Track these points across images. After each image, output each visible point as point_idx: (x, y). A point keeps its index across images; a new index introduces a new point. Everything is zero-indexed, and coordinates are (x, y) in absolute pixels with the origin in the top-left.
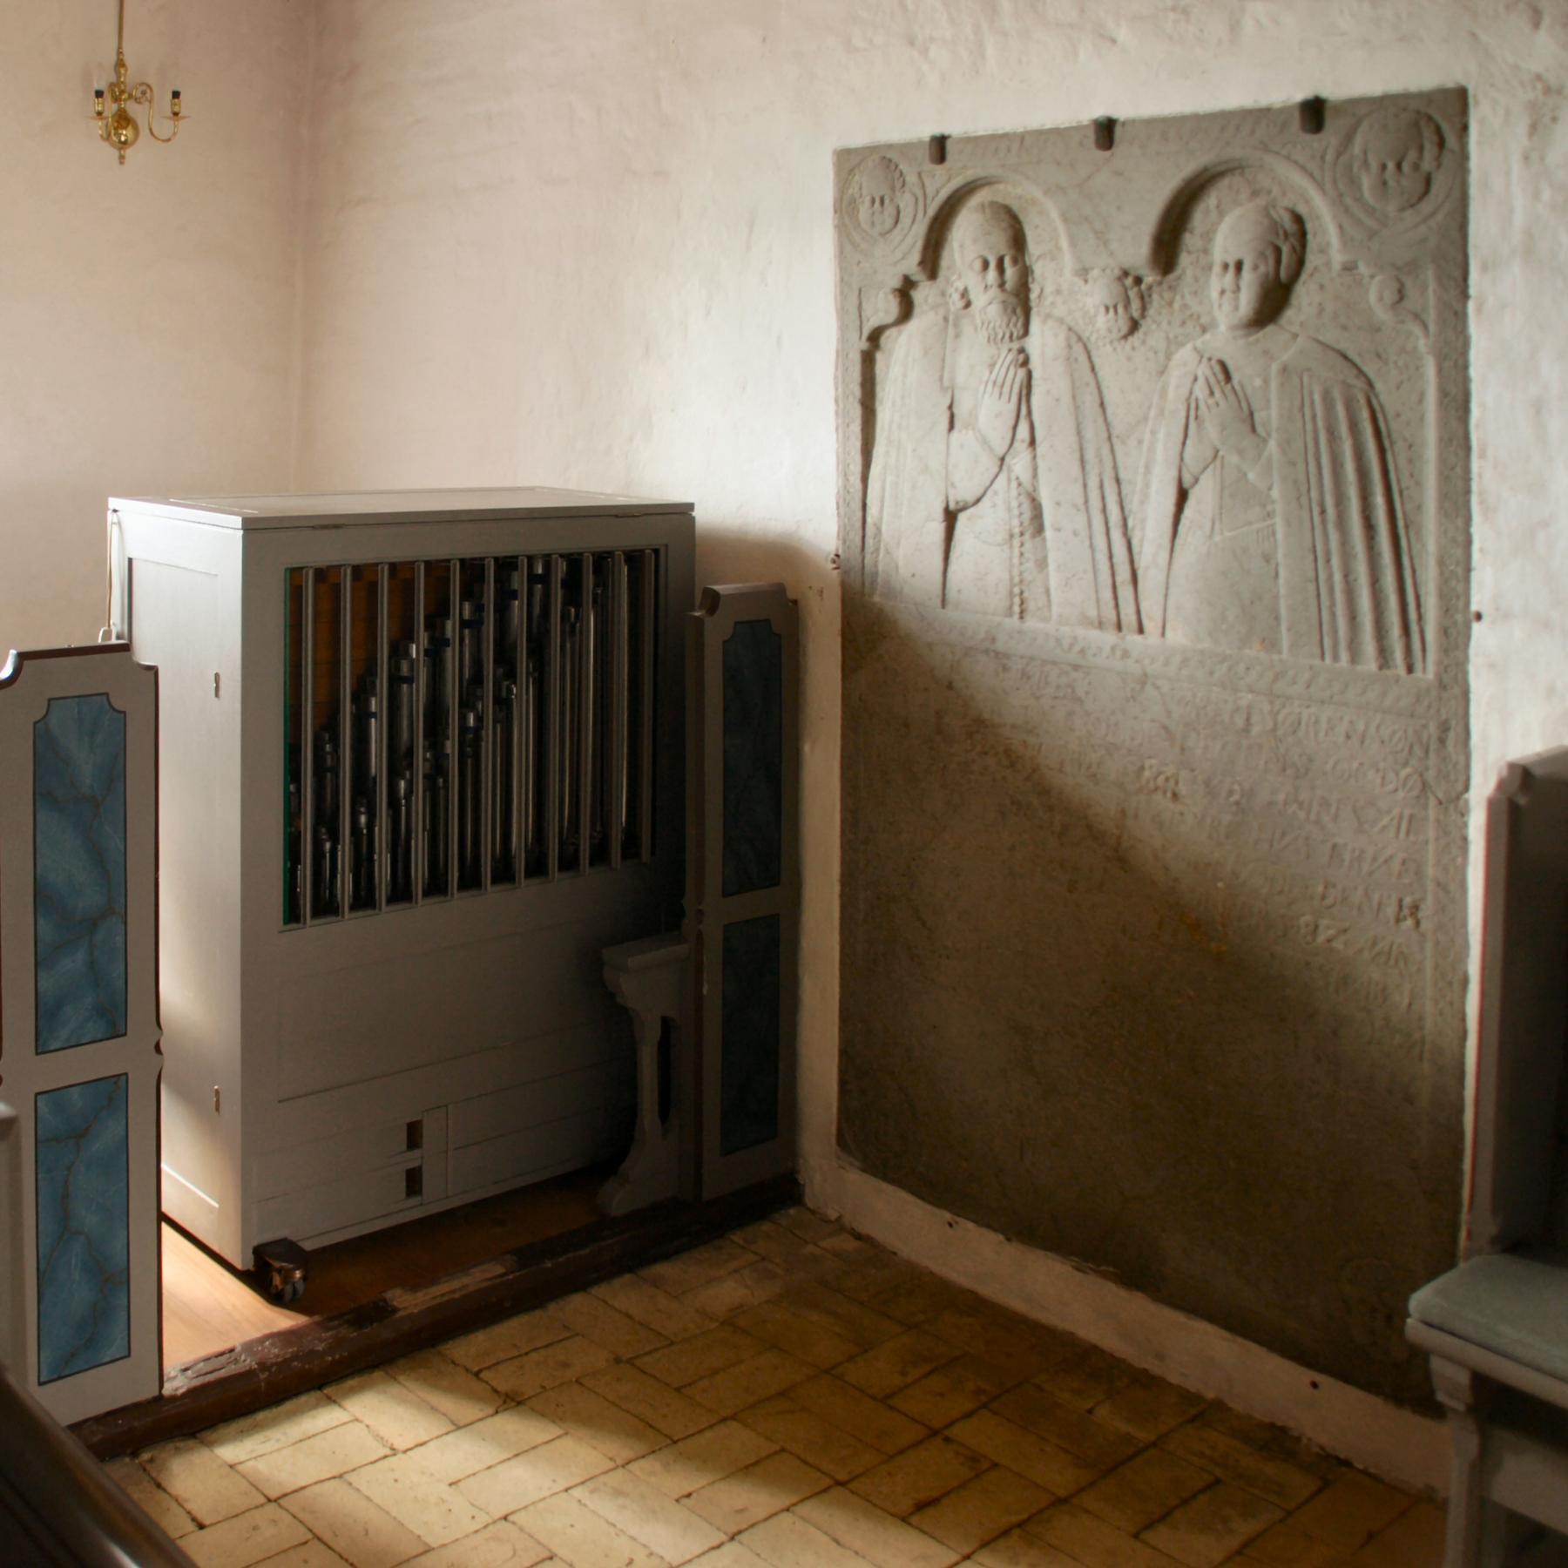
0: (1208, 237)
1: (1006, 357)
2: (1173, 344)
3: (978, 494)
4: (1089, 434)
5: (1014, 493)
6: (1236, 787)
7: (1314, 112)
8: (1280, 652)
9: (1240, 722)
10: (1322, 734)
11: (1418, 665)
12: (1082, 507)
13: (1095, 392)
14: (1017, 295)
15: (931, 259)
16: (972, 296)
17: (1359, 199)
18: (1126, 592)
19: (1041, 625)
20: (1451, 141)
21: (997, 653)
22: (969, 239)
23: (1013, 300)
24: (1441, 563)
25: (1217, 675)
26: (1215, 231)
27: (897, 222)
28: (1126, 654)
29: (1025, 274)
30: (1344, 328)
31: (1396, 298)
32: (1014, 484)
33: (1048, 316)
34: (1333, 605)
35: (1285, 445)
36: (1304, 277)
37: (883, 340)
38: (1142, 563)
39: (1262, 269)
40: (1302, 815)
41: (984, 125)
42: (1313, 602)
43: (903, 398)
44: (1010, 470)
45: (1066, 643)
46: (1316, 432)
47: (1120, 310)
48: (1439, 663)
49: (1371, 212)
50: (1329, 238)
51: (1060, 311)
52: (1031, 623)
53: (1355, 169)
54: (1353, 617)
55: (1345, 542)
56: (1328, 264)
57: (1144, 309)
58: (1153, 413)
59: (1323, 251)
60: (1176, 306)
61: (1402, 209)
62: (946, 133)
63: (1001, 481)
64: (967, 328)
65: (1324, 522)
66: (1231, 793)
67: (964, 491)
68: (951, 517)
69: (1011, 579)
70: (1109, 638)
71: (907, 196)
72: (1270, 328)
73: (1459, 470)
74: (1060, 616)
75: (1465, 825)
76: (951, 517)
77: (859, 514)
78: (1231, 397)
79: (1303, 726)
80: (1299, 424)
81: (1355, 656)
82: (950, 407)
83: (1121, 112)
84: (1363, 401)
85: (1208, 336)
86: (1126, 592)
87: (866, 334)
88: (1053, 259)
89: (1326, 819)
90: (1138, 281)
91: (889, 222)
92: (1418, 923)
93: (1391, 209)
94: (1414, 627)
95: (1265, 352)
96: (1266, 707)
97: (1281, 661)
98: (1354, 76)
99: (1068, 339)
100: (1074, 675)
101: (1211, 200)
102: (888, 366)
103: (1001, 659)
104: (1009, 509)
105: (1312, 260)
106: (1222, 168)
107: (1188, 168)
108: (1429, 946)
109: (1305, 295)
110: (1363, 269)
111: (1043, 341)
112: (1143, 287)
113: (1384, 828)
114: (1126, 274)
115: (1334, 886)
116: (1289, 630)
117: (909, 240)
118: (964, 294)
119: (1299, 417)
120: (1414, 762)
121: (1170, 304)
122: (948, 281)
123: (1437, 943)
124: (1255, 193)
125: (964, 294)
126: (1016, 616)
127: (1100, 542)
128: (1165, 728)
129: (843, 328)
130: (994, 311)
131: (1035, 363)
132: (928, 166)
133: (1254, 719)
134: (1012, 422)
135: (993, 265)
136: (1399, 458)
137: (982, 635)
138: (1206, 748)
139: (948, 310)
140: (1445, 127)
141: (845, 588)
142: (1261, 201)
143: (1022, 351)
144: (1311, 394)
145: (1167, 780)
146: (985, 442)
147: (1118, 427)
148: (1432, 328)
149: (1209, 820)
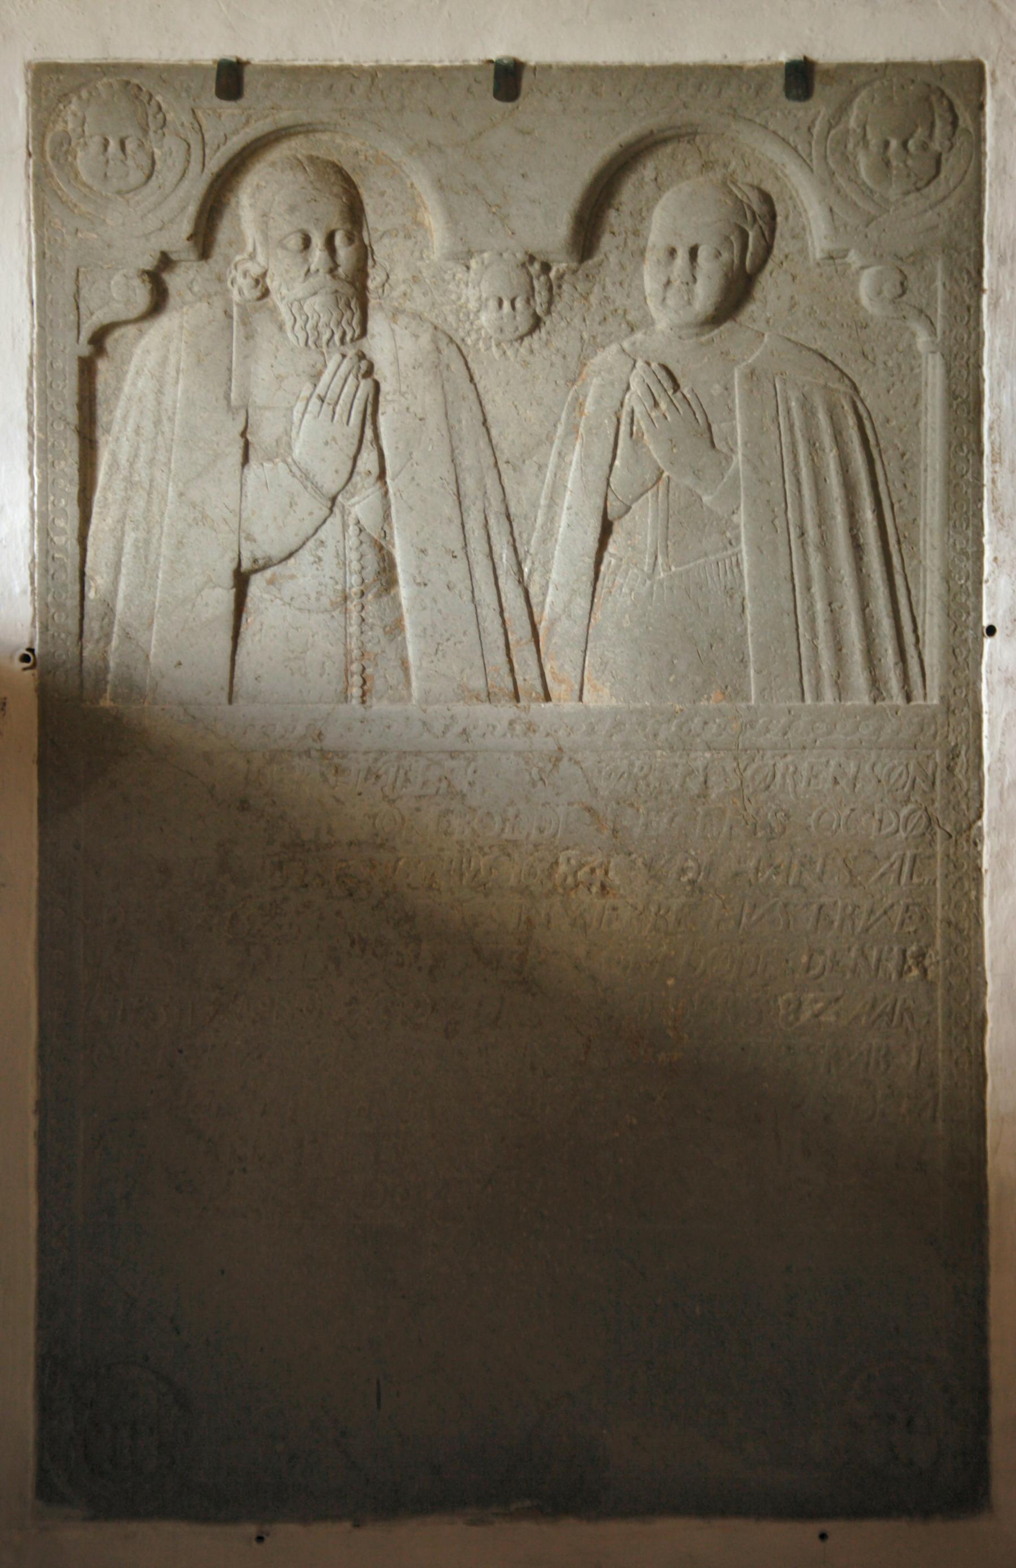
0: (642, 216)
1: (336, 367)
2: (591, 346)
3: (294, 547)
4: (467, 460)
5: (352, 541)
6: (690, 863)
7: (801, 77)
8: (747, 699)
9: (694, 786)
10: (803, 785)
11: (917, 692)
12: (460, 554)
13: (476, 408)
14: (352, 284)
15: (204, 238)
16: (272, 283)
17: (854, 179)
18: (524, 655)
19: (398, 707)
20: (965, 119)
21: (323, 753)
22: (265, 210)
23: (347, 290)
24: (947, 579)
25: (662, 736)
26: (650, 210)
27: (149, 177)
28: (531, 728)
29: (364, 255)
30: (822, 325)
31: (899, 291)
32: (352, 530)
33: (395, 314)
34: (814, 636)
35: (755, 460)
36: (770, 266)
37: (109, 343)
38: (547, 610)
39: (725, 256)
40: (778, 880)
41: (309, 53)
42: (790, 636)
43: (157, 423)
44: (343, 513)
45: (438, 727)
46: (793, 444)
47: (519, 304)
48: (945, 686)
49: (869, 194)
50: (812, 219)
51: (419, 302)
52: (378, 706)
53: (850, 146)
54: (838, 648)
55: (828, 566)
56: (803, 251)
57: (550, 302)
58: (560, 430)
59: (799, 234)
60: (593, 299)
61: (907, 193)
62: (244, 58)
63: (330, 531)
64: (264, 327)
65: (803, 545)
66: (683, 871)
67: (268, 540)
68: (241, 581)
69: (347, 653)
70: (507, 711)
71: (171, 142)
72: (728, 325)
73: (969, 476)
74: (427, 692)
75: (980, 854)
76: (241, 581)
77: (77, 588)
78: (682, 408)
79: (778, 776)
80: (774, 437)
81: (841, 689)
82: (243, 434)
83: (532, 55)
84: (847, 407)
85: (639, 336)
86: (524, 655)
87: (85, 335)
88: (408, 236)
89: (808, 878)
90: (546, 268)
91: (136, 177)
92: (925, 972)
93: (894, 193)
94: (911, 652)
95: (725, 354)
96: (730, 765)
97: (749, 708)
98: (849, 39)
99: (435, 341)
100: (450, 763)
101: (648, 170)
102: (120, 378)
103: (334, 762)
104: (344, 564)
105: (781, 246)
106: (668, 133)
107: (628, 133)
108: (940, 992)
109: (772, 289)
110: (854, 258)
111: (387, 342)
112: (552, 274)
113: (883, 875)
114: (532, 259)
115: (822, 952)
116: (758, 672)
117: (173, 202)
118: (259, 281)
119: (773, 428)
120: (916, 797)
121: (586, 297)
122: (228, 260)
123: (949, 988)
124: (706, 166)
125: (259, 281)
126: (355, 702)
127: (486, 594)
128: (589, 809)
129: (45, 327)
130: (318, 306)
131: (384, 371)
132: (210, 99)
133: (713, 779)
134: (353, 449)
135: (318, 241)
136: (889, 467)
137: (300, 730)
138: (647, 825)
139: (229, 302)
140: (958, 102)
141: (43, 691)
142: (718, 175)
143: (362, 356)
144: (787, 401)
145: (593, 871)
146: (306, 477)
147: (506, 449)
148: (939, 326)
149: (653, 909)
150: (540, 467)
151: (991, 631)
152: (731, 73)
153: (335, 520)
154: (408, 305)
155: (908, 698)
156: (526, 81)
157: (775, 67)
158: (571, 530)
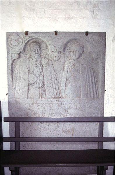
32: (40, 81)
62: (28, 31)
67: (31, 82)
69: (40, 93)
81: (88, 97)
107: (65, 41)
150: (60, 74)
151: (106, 91)
152: (80, 33)
153: (38, 80)
154: (46, 57)
155: (97, 98)
156: (58, 34)
157: (84, 32)
158: (63, 81)
